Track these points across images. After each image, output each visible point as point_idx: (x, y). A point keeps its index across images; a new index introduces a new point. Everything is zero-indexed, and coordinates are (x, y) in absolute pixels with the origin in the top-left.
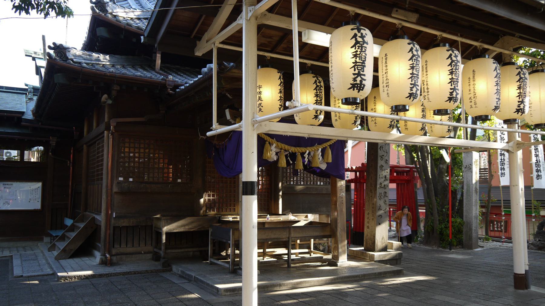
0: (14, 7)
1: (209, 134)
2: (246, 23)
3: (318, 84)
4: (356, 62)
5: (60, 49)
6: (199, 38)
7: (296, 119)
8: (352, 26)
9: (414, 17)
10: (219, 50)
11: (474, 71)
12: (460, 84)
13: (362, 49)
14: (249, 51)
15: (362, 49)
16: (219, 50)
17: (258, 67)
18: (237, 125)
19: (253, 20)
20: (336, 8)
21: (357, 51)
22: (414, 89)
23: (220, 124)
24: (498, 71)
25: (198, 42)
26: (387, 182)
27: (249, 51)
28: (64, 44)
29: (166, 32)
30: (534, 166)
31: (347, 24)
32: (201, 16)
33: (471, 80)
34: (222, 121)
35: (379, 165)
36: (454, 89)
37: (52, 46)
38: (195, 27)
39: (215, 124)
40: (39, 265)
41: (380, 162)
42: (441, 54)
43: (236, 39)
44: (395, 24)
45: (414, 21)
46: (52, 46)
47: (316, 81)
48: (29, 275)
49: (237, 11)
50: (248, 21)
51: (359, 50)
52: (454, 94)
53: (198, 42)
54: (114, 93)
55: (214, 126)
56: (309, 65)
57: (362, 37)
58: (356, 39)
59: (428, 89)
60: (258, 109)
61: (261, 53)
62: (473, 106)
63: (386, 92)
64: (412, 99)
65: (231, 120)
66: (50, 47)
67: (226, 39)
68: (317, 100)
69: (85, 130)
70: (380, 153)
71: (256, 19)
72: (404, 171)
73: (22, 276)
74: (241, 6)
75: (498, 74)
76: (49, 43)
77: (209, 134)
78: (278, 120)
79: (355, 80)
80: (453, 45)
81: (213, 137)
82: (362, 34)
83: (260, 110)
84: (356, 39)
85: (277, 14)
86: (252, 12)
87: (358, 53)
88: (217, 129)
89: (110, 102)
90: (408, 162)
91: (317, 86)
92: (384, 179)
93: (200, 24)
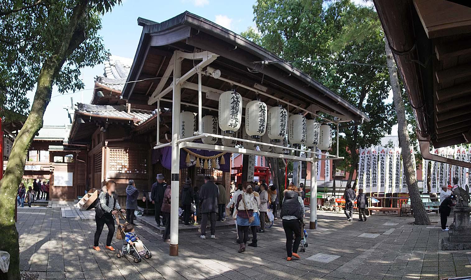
0: (59, 90)
1: (155, 148)
2: (175, 87)
3: (215, 121)
4: (233, 112)
5: (80, 106)
6: (150, 95)
7: (203, 140)
8: (232, 92)
9: (265, 89)
10: (161, 102)
11: (293, 121)
12: (286, 127)
13: (236, 105)
14: (176, 102)
15: (236, 105)
16: (161, 102)
17: (181, 112)
18: (169, 144)
19: (179, 85)
20: (224, 81)
21: (234, 106)
22: (262, 127)
23: (161, 142)
24: (305, 122)
25: (149, 97)
26: (252, 176)
27: (176, 102)
28: (83, 103)
29: (133, 93)
30: (326, 170)
31: (230, 90)
32: (151, 83)
33: (292, 125)
34: (163, 140)
35: (249, 166)
36: (283, 129)
37: (77, 104)
38: (150, 86)
39: (158, 143)
40: (73, 213)
41: (249, 165)
42: (278, 111)
43: (169, 96)
44: (255, 92)
45: (265, 91)
46: (77, 104)
47: (214, 120)
48: (69, 217)
49: (170, 80)
50: (176, 85)
51: (235, 105)
52: (283, 132)
53: (149, 97)
54: (106, 126)
55: (157, 144)
56: (210, 111)
57: (237, 98)
58: (234, 100)
59: (270, 128)
60: (182, 134)
61: (184, 103)
62: (292, 138)
63: (247, 128)
64: (260, 132)
65: (168, 140)
66: (75, 105)
67: (166, 95)
68: (214, 130)
69: (93, 146)
70: (250, 160)
71: (180, 85)
72: (264, 170)
73: (66, 217)
74: (172, 78)
75: (304, 123)
76: (75, 102)
77: (155, 148)
78: (193, 141)
79: (281, 131)
80: (285, 106)
81: (156, 149)
82: (237, 97)
83: (183, 135)
84: (234, 100)
85: (192, 82)
86: (178, 81)
87: (235, 107)
88: (159, 145)
89: (105, 131)
90: (266, 165)
91: (215, 122)
92: (251, 174)
93: (150, 88)
